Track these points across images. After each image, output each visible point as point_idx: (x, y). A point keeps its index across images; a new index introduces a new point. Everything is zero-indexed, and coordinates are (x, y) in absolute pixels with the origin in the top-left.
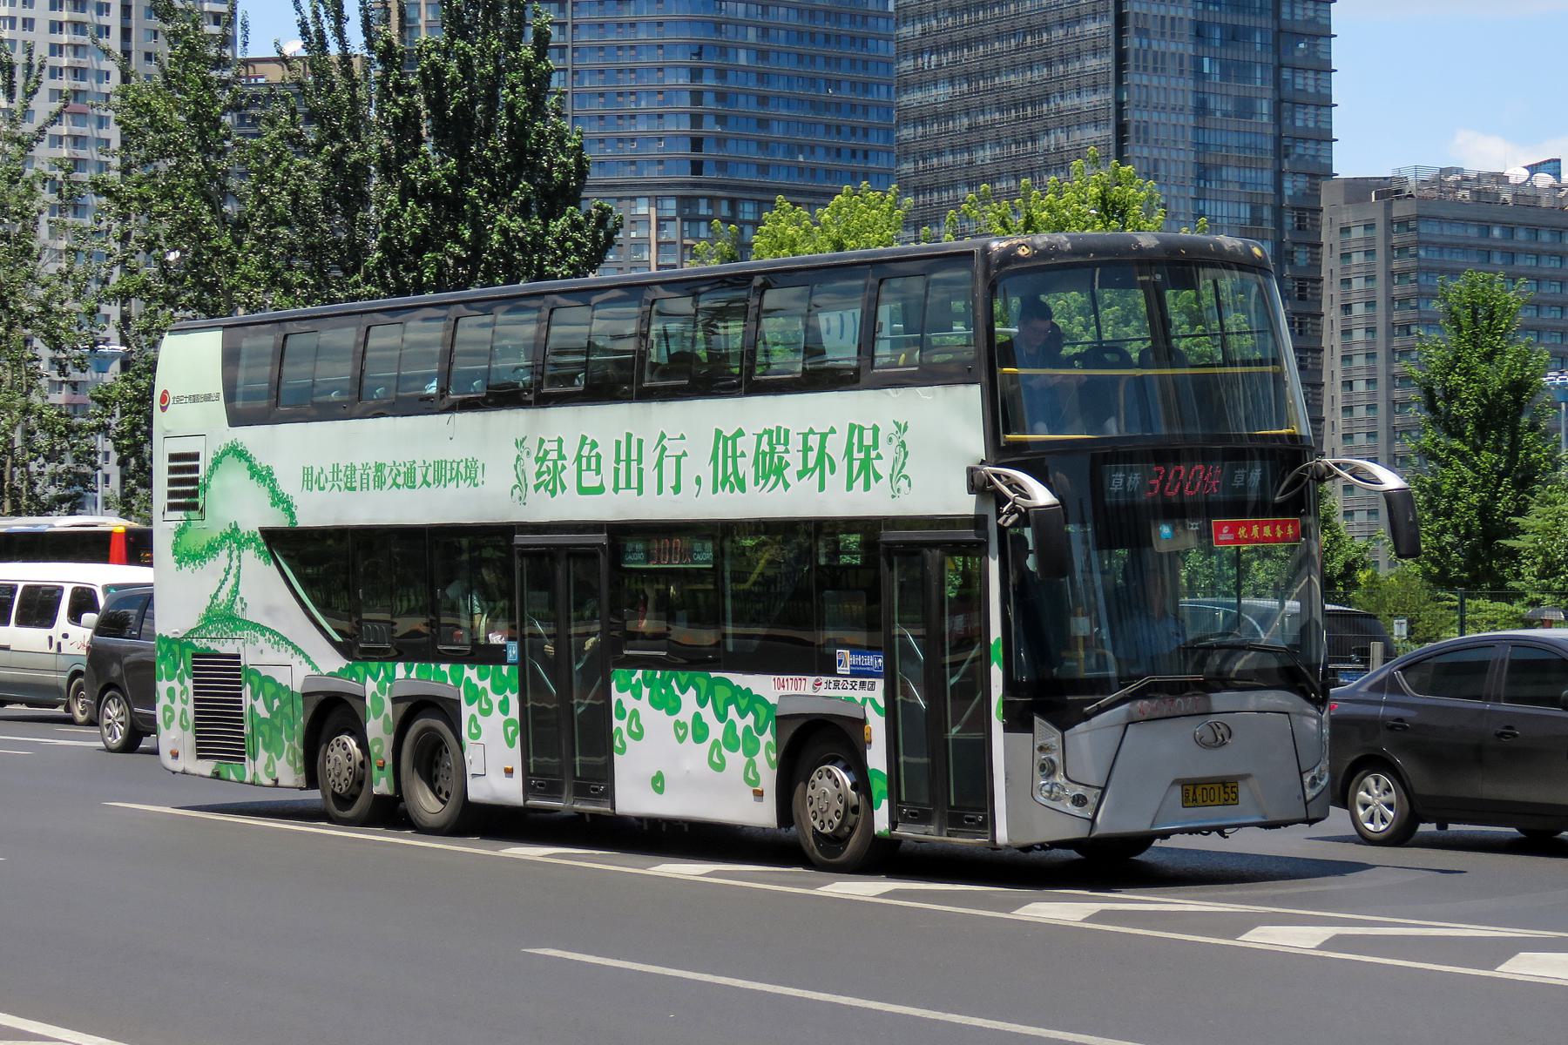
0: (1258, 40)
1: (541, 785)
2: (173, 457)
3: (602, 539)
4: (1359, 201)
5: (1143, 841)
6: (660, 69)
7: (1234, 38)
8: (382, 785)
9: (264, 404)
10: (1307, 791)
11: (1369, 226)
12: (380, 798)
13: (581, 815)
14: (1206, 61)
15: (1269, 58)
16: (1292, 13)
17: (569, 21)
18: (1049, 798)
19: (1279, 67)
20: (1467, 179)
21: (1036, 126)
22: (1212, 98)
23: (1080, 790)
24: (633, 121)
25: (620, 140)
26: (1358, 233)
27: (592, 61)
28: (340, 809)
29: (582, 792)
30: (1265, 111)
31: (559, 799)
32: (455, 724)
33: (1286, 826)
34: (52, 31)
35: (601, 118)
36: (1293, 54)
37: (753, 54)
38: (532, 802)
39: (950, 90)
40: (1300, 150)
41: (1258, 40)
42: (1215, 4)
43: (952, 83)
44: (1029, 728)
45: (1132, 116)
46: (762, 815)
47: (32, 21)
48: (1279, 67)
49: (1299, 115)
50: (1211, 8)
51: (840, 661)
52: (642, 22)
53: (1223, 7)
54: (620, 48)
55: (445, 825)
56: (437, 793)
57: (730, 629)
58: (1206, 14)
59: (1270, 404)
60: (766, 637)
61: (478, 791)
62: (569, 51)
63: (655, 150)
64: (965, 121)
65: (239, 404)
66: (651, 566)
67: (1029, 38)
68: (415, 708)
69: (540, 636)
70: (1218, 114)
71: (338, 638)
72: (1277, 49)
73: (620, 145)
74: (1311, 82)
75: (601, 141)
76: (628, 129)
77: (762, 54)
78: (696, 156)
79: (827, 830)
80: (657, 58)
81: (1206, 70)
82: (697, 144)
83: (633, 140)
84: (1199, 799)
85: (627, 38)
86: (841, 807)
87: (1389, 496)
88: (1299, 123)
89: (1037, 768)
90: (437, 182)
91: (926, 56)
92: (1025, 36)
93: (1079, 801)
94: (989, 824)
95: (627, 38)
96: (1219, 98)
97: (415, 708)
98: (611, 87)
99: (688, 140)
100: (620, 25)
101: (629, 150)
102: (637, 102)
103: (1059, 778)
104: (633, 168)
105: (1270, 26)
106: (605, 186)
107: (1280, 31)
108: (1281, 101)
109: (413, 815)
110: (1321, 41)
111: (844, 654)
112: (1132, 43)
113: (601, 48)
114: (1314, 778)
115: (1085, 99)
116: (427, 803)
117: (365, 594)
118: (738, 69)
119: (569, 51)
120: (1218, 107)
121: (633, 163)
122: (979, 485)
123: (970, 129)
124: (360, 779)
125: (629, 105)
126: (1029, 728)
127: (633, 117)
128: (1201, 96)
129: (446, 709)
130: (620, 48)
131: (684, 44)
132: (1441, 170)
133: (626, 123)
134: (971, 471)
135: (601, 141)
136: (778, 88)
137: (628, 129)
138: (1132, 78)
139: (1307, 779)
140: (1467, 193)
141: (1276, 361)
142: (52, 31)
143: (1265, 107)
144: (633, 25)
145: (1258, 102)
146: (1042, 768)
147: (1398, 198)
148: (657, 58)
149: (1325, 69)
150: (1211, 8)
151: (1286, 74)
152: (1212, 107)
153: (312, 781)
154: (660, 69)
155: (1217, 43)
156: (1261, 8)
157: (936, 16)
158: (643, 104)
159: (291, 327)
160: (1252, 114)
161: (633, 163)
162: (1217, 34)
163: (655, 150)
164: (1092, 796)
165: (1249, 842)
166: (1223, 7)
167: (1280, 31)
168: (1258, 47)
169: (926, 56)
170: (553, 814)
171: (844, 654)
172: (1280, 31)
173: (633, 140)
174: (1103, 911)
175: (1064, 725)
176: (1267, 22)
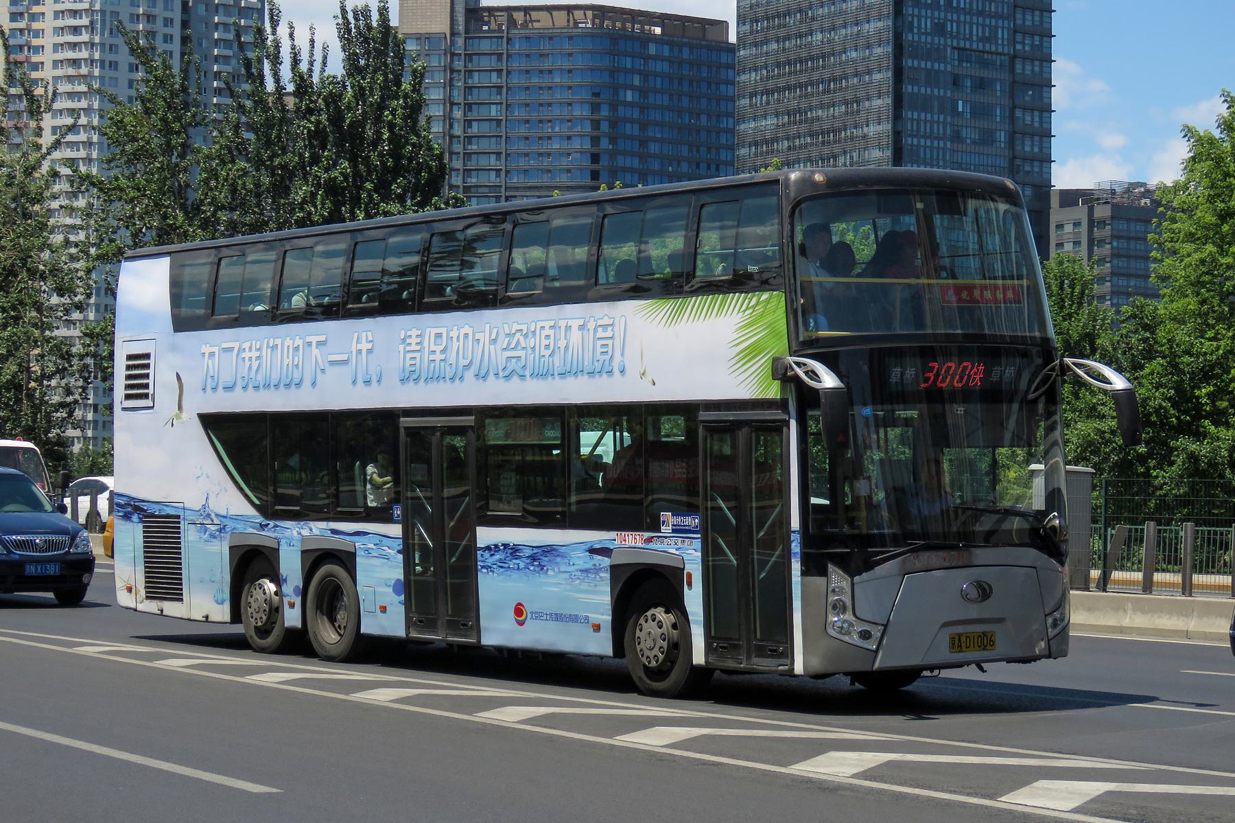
0: (998, 88)
1: (421, 621)
2: (130, 357)
3: (469, 420)
4: (1070, 205)
5: (913, 673)
6: (569, 104)
7: (980, 87)
8: (292, 617)
9: (201, 312)
10: (1050, 630)
11: (1077, 224)
12: (290, 632)
13: (451, 645)
14: (960, 103)
15: (1006, 101)
16: (1024, 68)
17: (505, 68)
18: (840, 633)
19: (1013, 108)
20: (1148, 191)
21: (837, 149)
22: (964, 130)
23: (866, 627)
24: (550, 141)
25: (540, 155)
26: (1069, 228)
27: (522, 97)
28: (261, 638)
29: (453, 626)
30: (1003, 140)
31: (435, 632)
32: (352, 572)
33: (1035, 661)
34: (131, 70)
35: (527, 138)
36: (1024, 98)
37: (637, 94)
38: (414, 634)
39: (775, 121)
40: (1027, 168)
41: (998, 88)
42: (967, 62)
43: (777, 116)
44: (823, 572)
45: (908, 141)
46: (600, 645)
47: (116, 63)
48: (1013, 108)
49: (1028, 143)
50: (965, 65)
51: (664, 522)
52: (555, 69)
53: (973, 64)
54: (541, 88)
55: (340, 655)
56: (337, 630)
57: (573, 499)
58: (960, 69)
59: (1024, 324)
60: (604, 500)
61: (369, 626)
62: (504, 90)
63: (565, 162)
64: (786, 143)
65: (184, 311)
66: (509, 442)
67: (832, 84)
68: (316, 559)
69: (419, 498)
70: (968, 141)
71: (257, 502)
72: (1012, 96)
73: (540, 159)
74: (1037, 119)
75: (527, 155)
76: (546, 146)
77: (643, 92)
78: (596, 167)
79: (654, 664)
80: (568, 96)
81: (960, 109)
82: (595, 158)
83: (549, 155)
84: (963, 645)
85: (546, 80)
86: (665, 644)
87: (1116, 396)
88: (1027, 149)
89: (830, 608)
90: (336, 178)
91: (759, 97)
92: (830, 83)
93: (865, 635)
94: (789, 654)
95: (546, 80)
96: (969, 130)
97: (316, 559)
98: (534, 116)
99: (589, 155)
100: (541, 72)
101: (546, 162)
102: (552, 128)
103: (849, 616)
104: (549, 175)
105: (1007, 78)
106: (530, 188)
107: (1014, 82)
108: (1015, 132)
109: (315, 645)
110: (1045, 89)
111: (666, 516)
112: (908, 88)
113: (527, 88)
114: (1055, 620)
115: (872, 128)
116: (328, 636)
117: (340, 467)
118: (626, 104)
119: (504, 90)
120: (969, 136)
121: (549, 171)
122: (781, 373)
123: (789, 148)
124: (275, 611)
125: (547, 129)
126: (823, 572)
127: (549, 138)
128: (956, 128)
129: (347, 560)
130: (541, 88)
131: (588, 86)
132: (1130, 184)
133: (545, 142)
134: (776, 360)
135: (527, 155)
136: (655, 116)
137: (546, 146)
138: (908, 114)
139: (1050, 620)
140: (1148, 201)
141: (1019, 302)
142: (131, 70)
143: (1002, 136)
144: (550, 72)
145: (998, 133)
146: (834, 607)
147: (1098, 204)
148: (568, 96)
149: (1046, 109)
150: (965, 65)
151: (1018, 113)
152: (964, 136)
153: (236, 616)
154: (569, 104)
155: (969, 91)
156: (1001, 65)
157: (766, 68)
158: (557, 129)
159: (225, 252)
160: (993, 141)
161: (549, 171)
162: (968, 83)
163: (565, 162)
164: (876, 632)
165: (1000, 673)
166: (973, 64)
167: (1014, 82)
168: (998, 93)
169: (759, 97)
170: (430, 646)
171: (666, 516)
172: (1013, 83)
173: (549, 155)
174: (889, 764)
175: (852, 572)
176: (1006, 76)
